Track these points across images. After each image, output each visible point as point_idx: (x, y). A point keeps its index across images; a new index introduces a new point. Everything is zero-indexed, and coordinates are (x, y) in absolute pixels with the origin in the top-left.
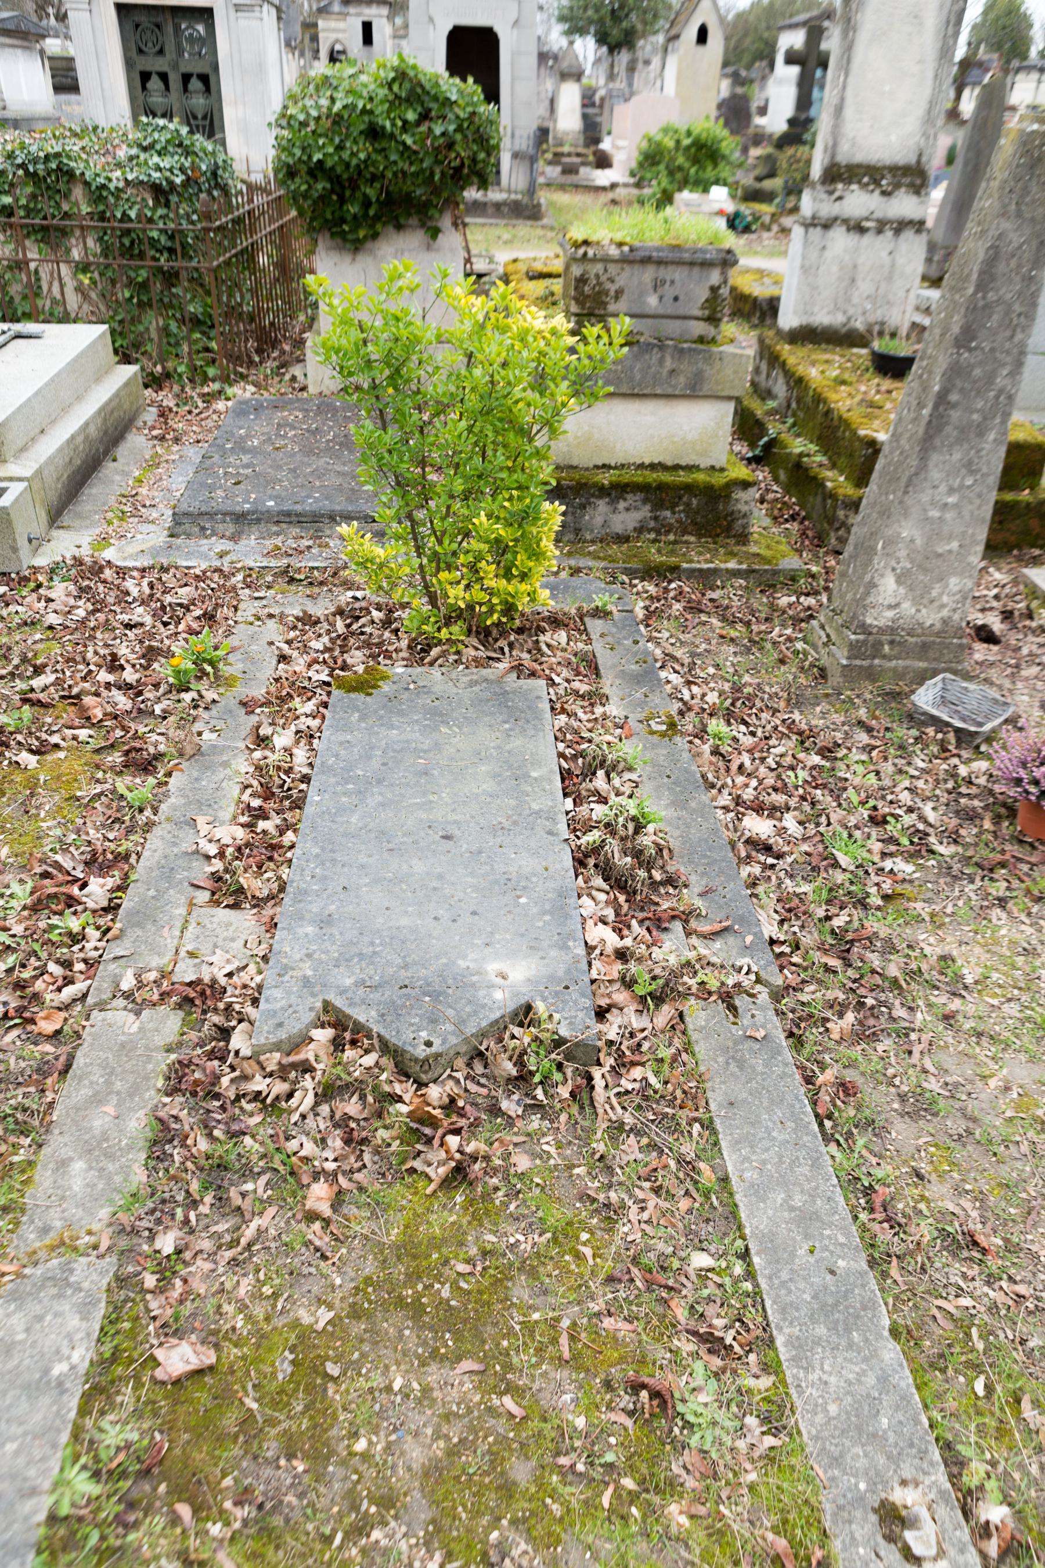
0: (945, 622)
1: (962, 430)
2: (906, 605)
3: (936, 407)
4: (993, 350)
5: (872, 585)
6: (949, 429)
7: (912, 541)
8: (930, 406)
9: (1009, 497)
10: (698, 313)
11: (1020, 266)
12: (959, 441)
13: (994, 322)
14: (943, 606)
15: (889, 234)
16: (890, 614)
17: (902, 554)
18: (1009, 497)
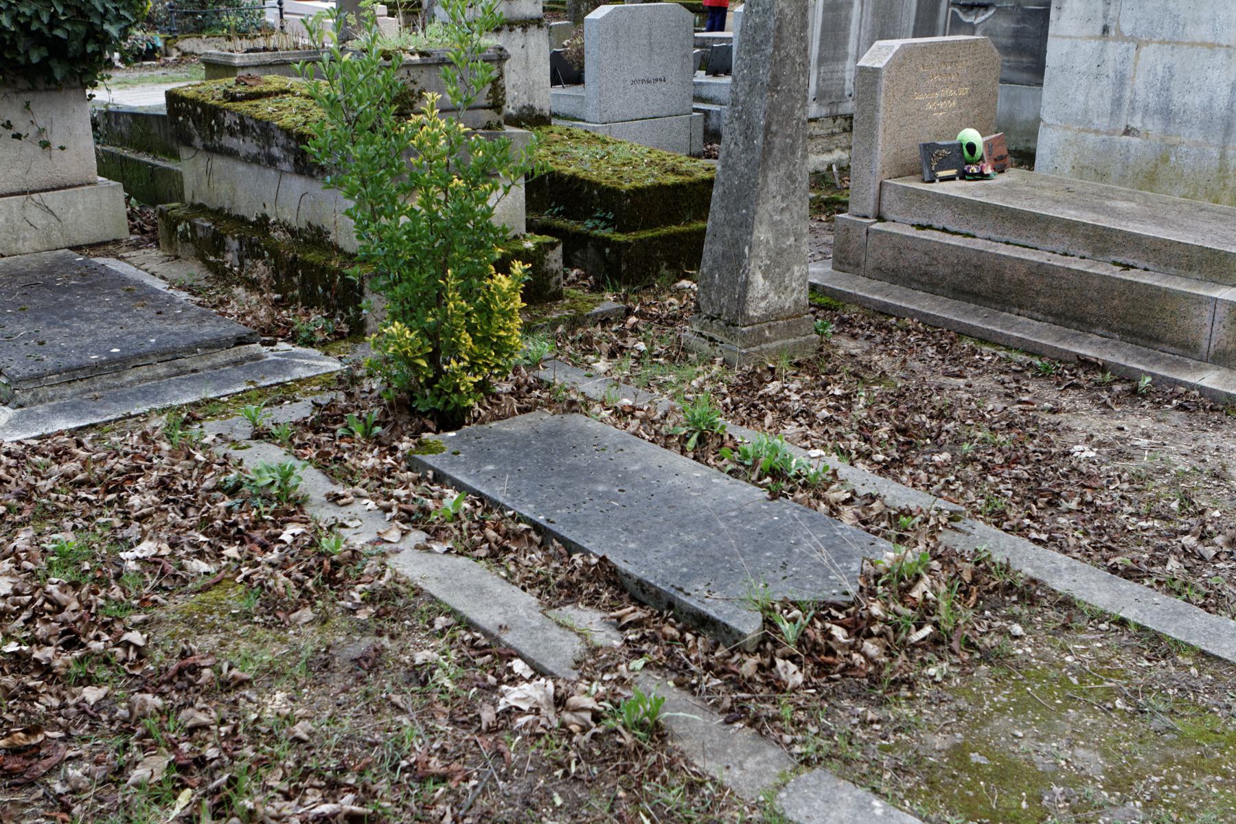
0: (796, 302)
1: (782, 151)
2: (771, 295)
3: (765, 137)
4: (790, 91)
5: (746, 284)
6: (775, 151)
7: (768, 242)
8: (761, 136)
9: (701, 225)
10: (484, 102)
11: (794, 31)
12: (782, 161)
13: (787, 71)
14: (793, 290)
15: (519, 30)
16: (763, 304)
17: (763, 254)
18: (701, 225)
